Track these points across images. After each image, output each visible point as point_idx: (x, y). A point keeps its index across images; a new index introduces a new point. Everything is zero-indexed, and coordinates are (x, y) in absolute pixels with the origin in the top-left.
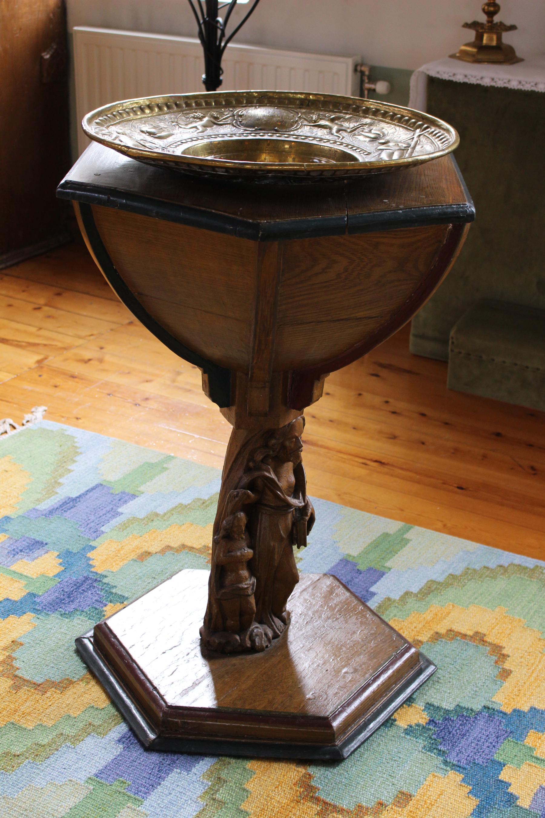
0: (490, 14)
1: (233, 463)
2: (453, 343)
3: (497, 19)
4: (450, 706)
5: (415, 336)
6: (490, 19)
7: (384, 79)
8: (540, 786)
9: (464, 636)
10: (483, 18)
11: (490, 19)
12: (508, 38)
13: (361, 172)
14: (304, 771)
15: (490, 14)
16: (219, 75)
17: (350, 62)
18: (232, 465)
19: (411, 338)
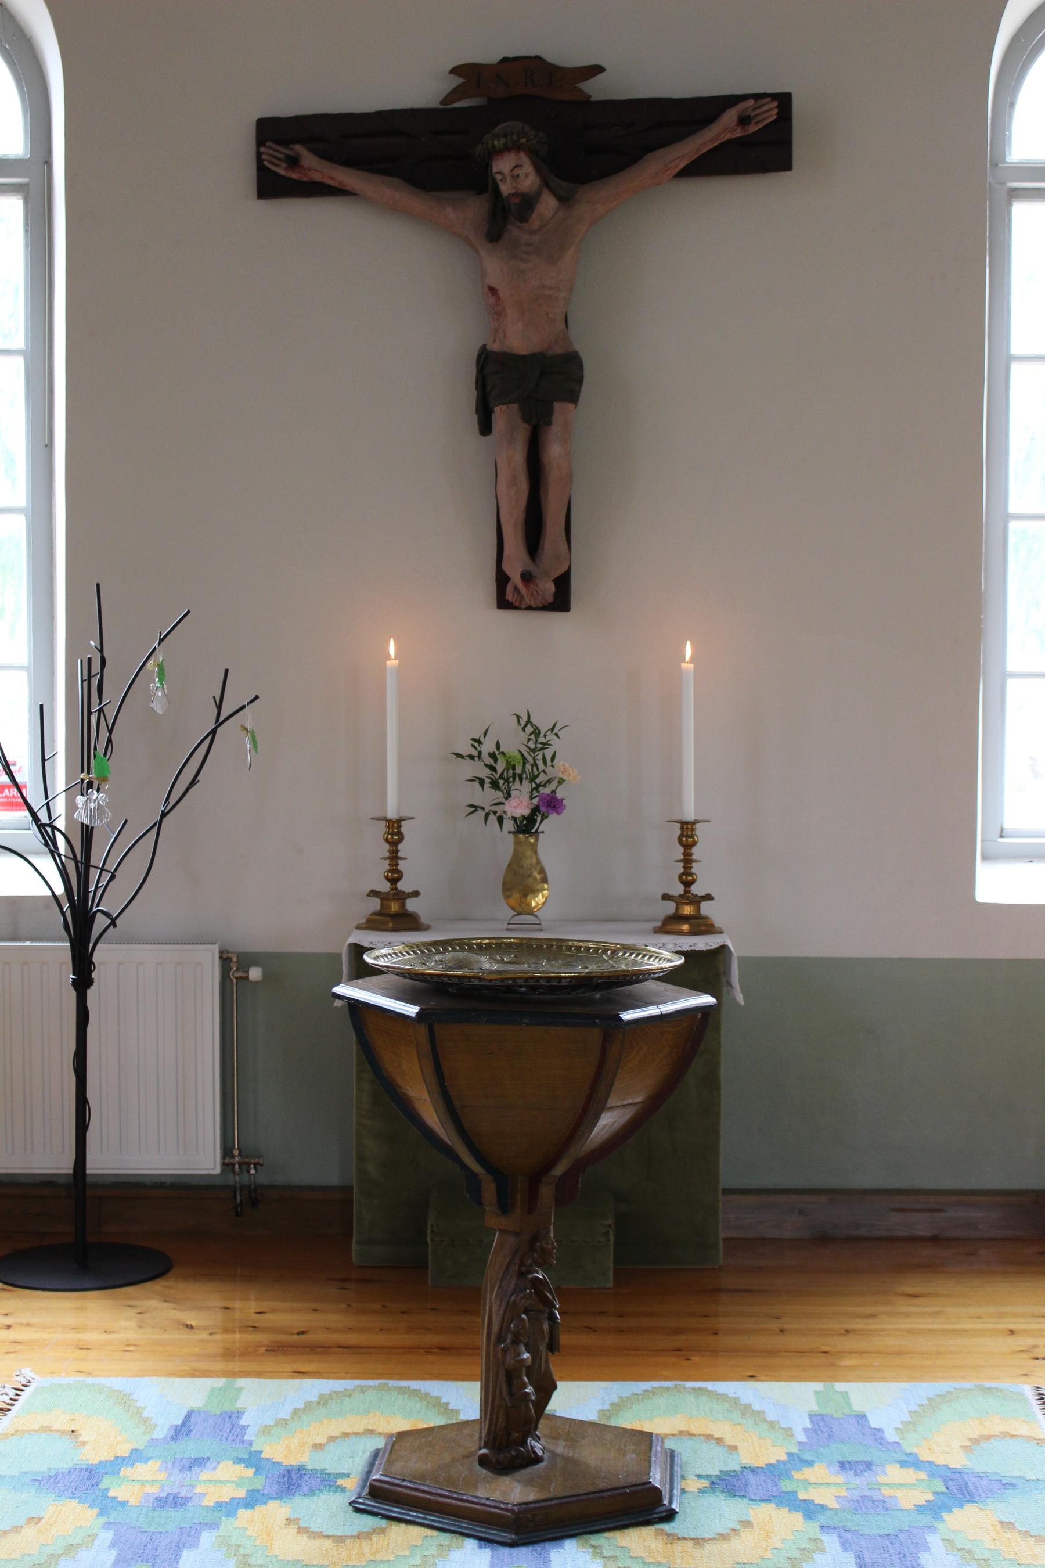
0: (394, 881)
1: (504, 1273)
2: (432, 1232)
3: (400, 885)
4: (717, 1473)
5: (358, 1243)
6: (393, 886)
7: (256, 965)
8: (835, 1496)
9: (673, 1435)
10: (385, 887)
11: (393, 886)
12: (411, 905)
13: (620, 978)
14: (653, 1528)
15: (394, 881)
16: (90, 972)
17: (216, 949)
18: (503, 1274)
19: (354, 1247)
